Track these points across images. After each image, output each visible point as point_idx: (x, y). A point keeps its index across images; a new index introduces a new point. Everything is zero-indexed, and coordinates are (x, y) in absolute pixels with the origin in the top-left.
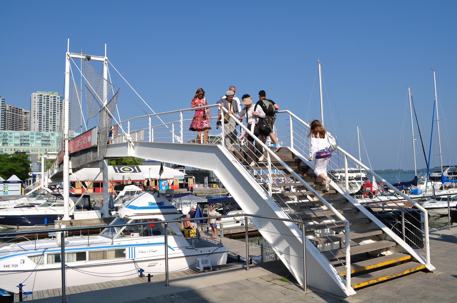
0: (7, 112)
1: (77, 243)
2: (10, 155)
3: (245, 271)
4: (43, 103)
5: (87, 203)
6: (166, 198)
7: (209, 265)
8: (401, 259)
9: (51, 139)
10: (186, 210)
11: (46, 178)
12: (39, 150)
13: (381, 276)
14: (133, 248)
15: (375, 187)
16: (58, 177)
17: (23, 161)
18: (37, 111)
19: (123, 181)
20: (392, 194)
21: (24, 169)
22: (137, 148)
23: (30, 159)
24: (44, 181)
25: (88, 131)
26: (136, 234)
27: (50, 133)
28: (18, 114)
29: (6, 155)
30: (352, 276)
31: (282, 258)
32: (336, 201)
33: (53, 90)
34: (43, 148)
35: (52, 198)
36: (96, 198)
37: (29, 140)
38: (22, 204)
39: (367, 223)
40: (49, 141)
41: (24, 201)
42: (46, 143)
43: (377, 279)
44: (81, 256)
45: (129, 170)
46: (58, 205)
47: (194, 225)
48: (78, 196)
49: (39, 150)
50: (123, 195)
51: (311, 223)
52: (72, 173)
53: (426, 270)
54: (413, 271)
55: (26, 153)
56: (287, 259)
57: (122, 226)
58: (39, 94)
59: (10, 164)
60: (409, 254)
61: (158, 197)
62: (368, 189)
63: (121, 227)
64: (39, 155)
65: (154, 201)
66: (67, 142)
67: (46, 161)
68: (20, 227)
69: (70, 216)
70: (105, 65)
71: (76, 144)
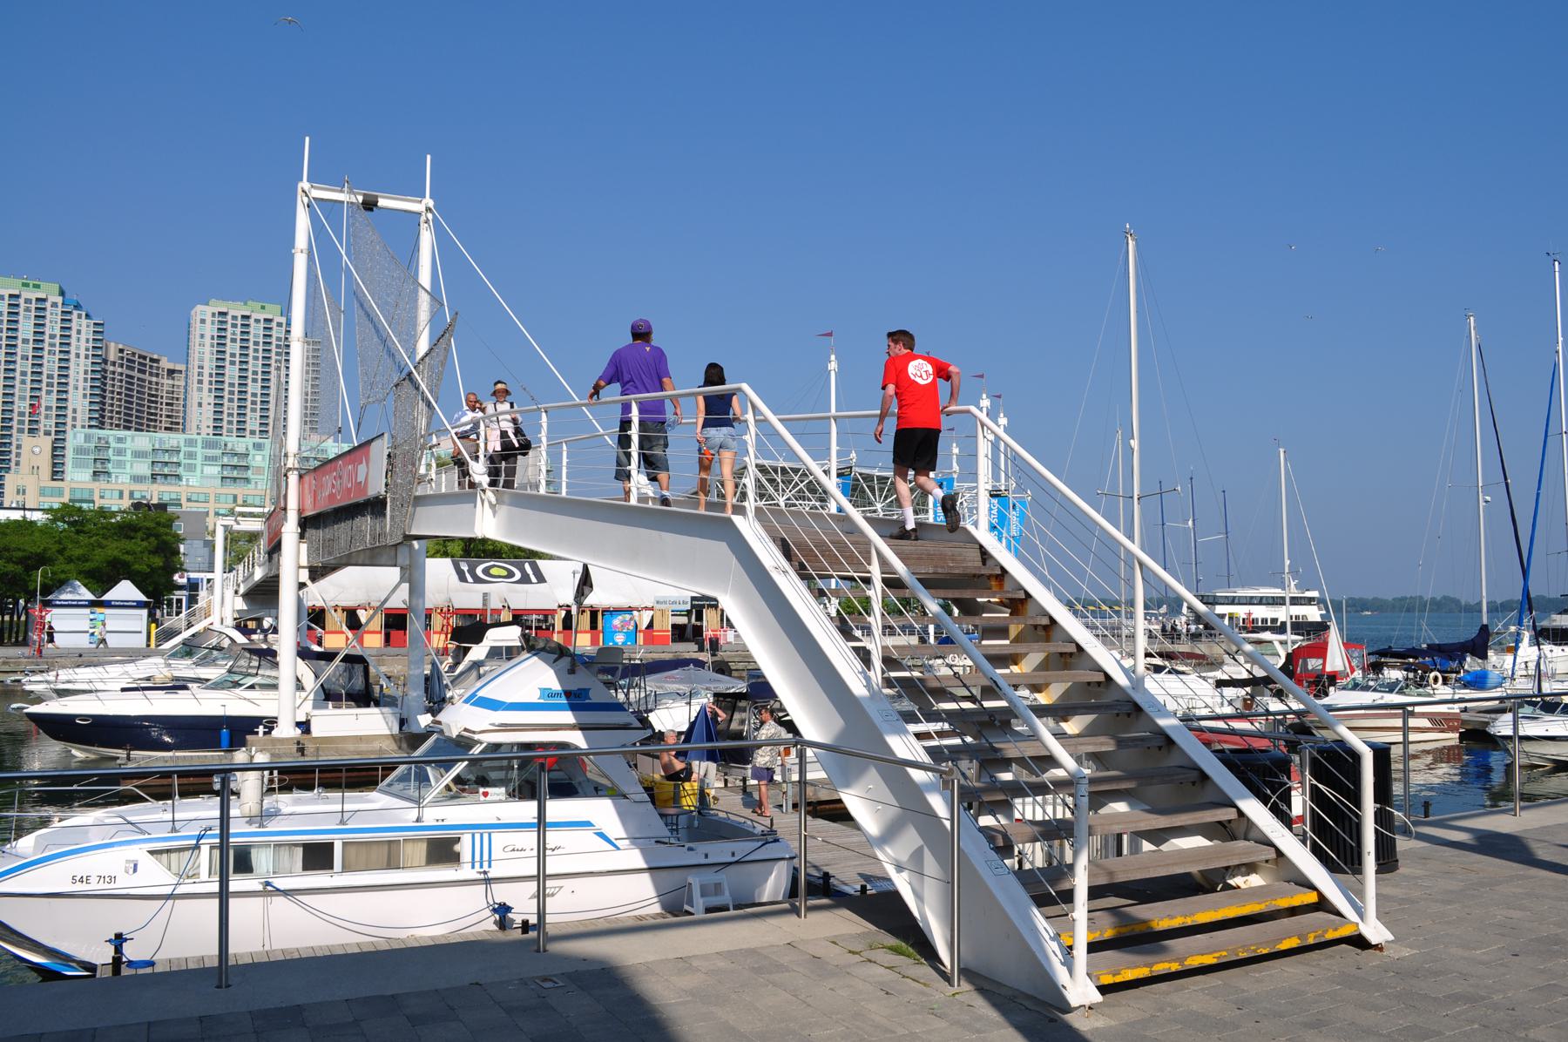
0: (112, 368)
1: (310, 813)
2: (114, 514)
3: (794, 918)
4: (228, 341)
5: (359, 683)
6: (598, 676)
7: (726, 898)
8: (1284, 903)
9: (253, 464)
10: (672, 718)
11: (229, 593)
12: (212, 498)
13: (1198, 952)
14: (486, 837)
15: (1336, 659)
16: (264, 594)
17: (157, 536)
18: (209, 366)
19: (483, 612)
20: (1391, 687)
21: (158, 561)
22: (503, 510)
23: (180, 528)
24: (221, 603)
25: (360, 446)
26: (498, 792)
27: (249, 441)
28: (147, 377)
29: (103, 513)
30: (1093, 947)
31: (902, 884)
32: (1108, 707)
33: (33, 277)
34: (225, 491)
35: (242, 662)
36: (389, 668)
37: (179, 464)
38: (148, 679)
39: (1194, 783)
40: (247, 468)
41: (154, 667)
42: (235, 474)
43: (1181, 960)
44: (317, 856)
45: (505, 573)
46: (264, 687)
47: (702, 768)
48: (329, 656)
49: (212, 498)
50: (482, 657)
51: (1007, 776)
52: (309, 583)
53: (1359, 942)
54: (1311, 941)
55: (170, 509)
56: (917, 887)
57: (452, 763)
58: (216, 310)
59: (115, 545)
60: (1312, 887)
61: (572, 671)
62: (1313, 663)
63: (447, 765)
64: (212, 514)
65: (556, 686)
66: (293, 478)
67: (232, 538)
68: (134, 753)
69: (299, 724)
70: (423, 226)
71: (320, 486)
